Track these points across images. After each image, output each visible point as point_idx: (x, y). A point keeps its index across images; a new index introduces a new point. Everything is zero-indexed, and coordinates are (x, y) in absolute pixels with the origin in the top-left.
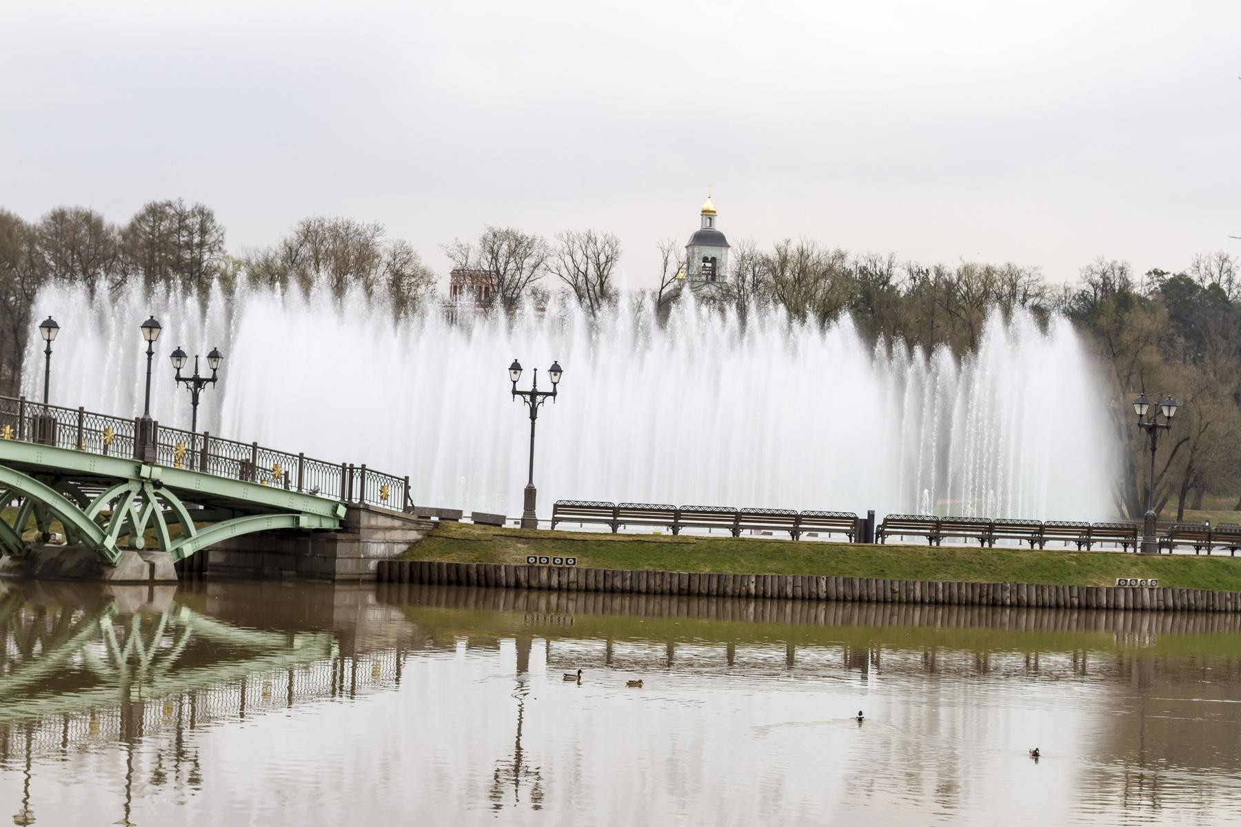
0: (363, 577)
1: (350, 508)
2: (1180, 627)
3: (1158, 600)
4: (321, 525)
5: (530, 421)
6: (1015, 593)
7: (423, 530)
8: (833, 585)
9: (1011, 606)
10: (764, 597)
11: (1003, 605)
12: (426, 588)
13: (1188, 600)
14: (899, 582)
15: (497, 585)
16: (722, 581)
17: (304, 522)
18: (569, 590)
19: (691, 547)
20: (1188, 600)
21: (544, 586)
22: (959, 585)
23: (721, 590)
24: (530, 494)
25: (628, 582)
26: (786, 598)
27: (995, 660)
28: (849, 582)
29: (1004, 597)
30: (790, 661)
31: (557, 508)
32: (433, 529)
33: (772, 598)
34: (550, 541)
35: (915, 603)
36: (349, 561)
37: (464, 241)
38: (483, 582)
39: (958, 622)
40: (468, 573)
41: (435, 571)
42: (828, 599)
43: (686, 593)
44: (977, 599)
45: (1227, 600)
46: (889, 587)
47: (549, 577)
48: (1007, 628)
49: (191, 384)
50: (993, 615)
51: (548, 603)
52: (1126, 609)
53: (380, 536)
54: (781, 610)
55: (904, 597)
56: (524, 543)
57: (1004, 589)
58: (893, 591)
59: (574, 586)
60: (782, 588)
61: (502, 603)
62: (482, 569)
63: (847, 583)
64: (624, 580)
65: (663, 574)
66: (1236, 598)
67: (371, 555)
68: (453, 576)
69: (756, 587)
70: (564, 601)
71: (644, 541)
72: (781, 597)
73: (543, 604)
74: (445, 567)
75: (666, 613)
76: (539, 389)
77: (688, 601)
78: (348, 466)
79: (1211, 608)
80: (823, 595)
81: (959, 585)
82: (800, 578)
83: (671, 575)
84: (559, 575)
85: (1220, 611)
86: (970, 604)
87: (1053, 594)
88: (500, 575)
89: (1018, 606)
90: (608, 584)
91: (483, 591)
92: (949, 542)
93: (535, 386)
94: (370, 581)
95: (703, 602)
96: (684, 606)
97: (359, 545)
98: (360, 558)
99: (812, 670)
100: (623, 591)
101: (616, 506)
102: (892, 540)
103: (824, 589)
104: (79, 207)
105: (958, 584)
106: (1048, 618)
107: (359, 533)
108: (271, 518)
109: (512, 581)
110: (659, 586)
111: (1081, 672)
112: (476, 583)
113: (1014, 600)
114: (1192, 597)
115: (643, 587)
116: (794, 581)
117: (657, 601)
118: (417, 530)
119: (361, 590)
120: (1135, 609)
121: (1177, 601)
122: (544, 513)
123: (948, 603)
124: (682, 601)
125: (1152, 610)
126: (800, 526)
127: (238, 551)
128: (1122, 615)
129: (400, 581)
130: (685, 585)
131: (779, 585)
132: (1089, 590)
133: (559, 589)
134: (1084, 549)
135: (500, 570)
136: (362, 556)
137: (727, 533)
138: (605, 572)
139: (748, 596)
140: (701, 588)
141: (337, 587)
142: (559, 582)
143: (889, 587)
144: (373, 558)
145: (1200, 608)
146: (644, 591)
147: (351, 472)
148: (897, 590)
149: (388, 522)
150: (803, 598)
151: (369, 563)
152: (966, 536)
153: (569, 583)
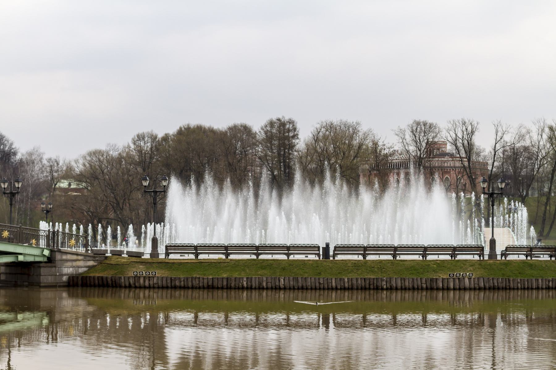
0: (59, 284)
2: (489, 299)
3: (474, 284)
4: (35, 260)
6: (389, 282)
7: (97, 260)
8: (287, 281)
9: (387, 289)
11: (382, 289)
12: (89, 288)
13: (493, 283)
14: (323, 278)
15: (121, 287)
17: (21, 258)
18: (154, 288)
19: (225, 264)
20: (493, 283)
21: (142, 286)
22: (357, 279)
23: (229, 285)
25: (182, 283)
26: (263, 288)
29: (382, 285)
30: (424, 320)
31: (335, 247)
32: (104, 260)
33: (255, 288)
34: (157, 264)
35: (332, 289)
36: (50, 276)
38: (114, 285)
39: (357, 298)
41: (92, 280)
42: (285, 289)
43: (211, 287)
44: (367, 286)
46: (317, 281)
47: (144, 281)
48: (385, 300)
49: (9, 195)
50: (377, 294)
51: (144, 294)
52: (454, 289)
53: (69, 264)
54: (260, 295)
55: (326, 286)
56: (143, 265)
58: (320, 284)
60: (261, 283)
61: (123, 295)
63: (295, 280)
64: (180, 282)
65: (199, 278)
69: (247, 283)
70: (151, 293)
71: (203, 262)
72: (261, 288)
73: (142, 295)
74: (96, 278)
75: (201, 297)
80: (282, 286)
81: (357, 279)
82: (270, 278)
83: (203, 279)
84: (149, 280)
85: (514, 289)
86: (363, 289)
87: (410, 282)
89: (390, 289)
90: (173, 284)
91: (114, 290)
94: (64, 286)
95: (220, 291)
96: (210, 294)
97: (55, 269)
98: (56, 275)
99: (434, 324)
100: (180, 288)
101: (396, 246)
102: (339, 257)
103: (283, 283)
104: (242, 123)
105: (356, 278)
106: (408, 295)
107: (55, 263)
108: (2, 257)
109: (127, 284)
110: (198, 284)
112: (111, 285)
113: (388, 286)
114: (495, 281)
116: (267, 279)
117: (197, 292)
118: (94, 261)
120: (460, 289)
121: (486, 284)
122: (161, 250)
125: (470, 289)
126: (427, 252)
127: (10, 274)
128: (452, 292)
130: (210, 283)
131: (259, 282)
132: (432, 280)
133: (149, 287)
136: (58, 274)
137: (390, 257)
139: (243, 288)
141: (42, 289)
142: (149, 284)
143: (317, 281)
144: (65, 275)
145: (195, 287)
148: (322, 282)
149: (75, 257)
150: (272, 288)
153: (154, 284)
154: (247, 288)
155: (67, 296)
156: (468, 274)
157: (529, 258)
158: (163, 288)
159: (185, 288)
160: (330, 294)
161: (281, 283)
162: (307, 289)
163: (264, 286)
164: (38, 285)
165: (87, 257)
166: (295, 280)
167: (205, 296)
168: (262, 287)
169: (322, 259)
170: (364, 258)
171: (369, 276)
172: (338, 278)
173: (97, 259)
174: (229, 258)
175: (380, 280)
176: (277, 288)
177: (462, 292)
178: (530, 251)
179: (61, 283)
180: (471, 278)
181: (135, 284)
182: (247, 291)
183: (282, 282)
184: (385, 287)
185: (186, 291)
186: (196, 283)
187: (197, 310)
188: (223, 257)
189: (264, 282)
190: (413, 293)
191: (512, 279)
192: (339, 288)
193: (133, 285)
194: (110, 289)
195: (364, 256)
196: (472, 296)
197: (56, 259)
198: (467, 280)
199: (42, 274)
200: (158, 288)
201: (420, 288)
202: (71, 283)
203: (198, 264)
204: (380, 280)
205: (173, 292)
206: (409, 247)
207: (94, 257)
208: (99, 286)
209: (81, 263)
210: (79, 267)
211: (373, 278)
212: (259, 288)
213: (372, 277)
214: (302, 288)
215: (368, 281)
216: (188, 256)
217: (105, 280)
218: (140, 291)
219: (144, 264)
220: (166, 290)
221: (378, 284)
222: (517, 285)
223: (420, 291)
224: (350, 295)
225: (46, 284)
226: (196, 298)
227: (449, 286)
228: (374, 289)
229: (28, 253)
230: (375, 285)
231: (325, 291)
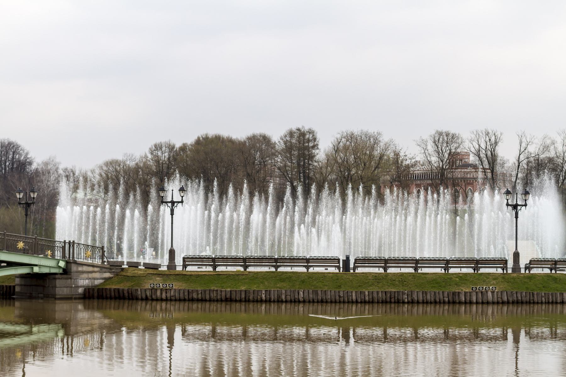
0: (74, 296)
1: (67, 263)
2: (512, 312)
3: (497, 298)
4: (50, 271)
5: (171, 216)
7: (114, 272)
8: (306, 294)
10: (270, 301)
11: (404, 303)
12: (105, 301)
13: (517, 297)
15: (137, 299)
16: (247, 294)
17: (36, 270)
18: (171, 300)
20: (517, 297)
21: (159, 299)
22: (378, 292)
23: (247, 298)
24: (172, 253)
26: (282, 301)
27: (251, 330)
28: (316, 292)
32: (120, 272)
33: (274, 301)
37: (424, 138)
38: (131, 297)
40: (123, 293)
41: (108, 293)
42: (304, 302)
43: (229, 300)
44: (388, 300)
45: (542, 297)
46: (337, 294)
47: (161, 294)
48: (406, 315)
50: (398, 307)
51: (161, 306)
52: (477, 303)
53: (85, 275)
54: (279, 308)
55: (346, 299)
56: (160, 277)
57: (403, 293)
58: (340, 296)
59: (173, 298)
62: (130, 291)
63: (314, 293)
64: (198, 294)
65: (217, 290)
66: (548, 296)
67: (79, 285)
68: (117, 295)
69: (265, 296)
70: (168, 306)
71: (221, 274)
72: (279, 301)
73: (158, 307)
75: (219, 310)
76: (175, 200)
77: (231, 305)
78: (72, 242)
79: (532, 301)
80: (301, 299)
81: (378, 292)
83: (221, 291)
84: (166, 293)
85: (538, 303)
86: (384, 302)
87: (432, 296)
88: (138, 294)
90: (190, 297)
91: (131, 302)
92: (536, 271)
93: (172, 198)
94: (80, 298)
96: (228, 307)
100: (198, 300)
102: (360, 270)
106: (429, 308)
107: (71, 275)
108: (17, 268)
109: (144, 296)
110: (215, 297)
111: (554, 336)
112: (127, 298)
113: (410, 299)
114: (519, 295)
115: (208, 297)
117: (215, 305)
118: (110, 272)
119: (73, 303)
120: (483, 303)
121: (509, 298)
122: (179, 261)
123: (371, 302)
124: (228, 304)
125: (493, 303)
126: (449, 265)
127: (25, 285)
129: (94, 298)
130: (228, 296)
131: (278, 295)
132: (454, 294)
133: (166, 300)
134: (553, 272)
135: (138, 291)
136: (73, 286)
137: (411, 270)
138: (188, 291)
139: (262, 301)
140: (237, 297)
141: (57, 302)
142: (166, 296)
144: (81, 287)
146: (208, 300)
147: (73, 246)
148: (342, 295)
149: (91, 269)
151: (78, 289)
152: (543, 267)
153: (171, 297)
155: (83, 308)
156: (491, 287)
157: (553, 272)
158: (180, 300)
159: (203, 300)
160: (350, 308)
162: (327, 302)
163: (283, 299)
165: (103, 269)
166: (314, 293)
169: (343, 271)
170: (385, 271)
172: (358, 291)
173: (113, 270)
174: (247, 270)
175: (401, 293)
176: (296, 302)
177: (485, 306)
179: (77, 295)
180: (494, 292)
183: (301, 295)
184: (406, 300)
185: (204, 304)
186: (213, 295)
188: (241, 269)
189: (283, 295)
192: (360, 301)
193: (150, 298)
195: (385, 269)
197: (72, 271)
198: (490, 294)
200: (176, 300)
201: (442, 301)
204: (401, 293)
205: (190, 305)
207: (111, 269)
208: (115, 298)
209: (97, 275)
210: (95, 279)
212: (278, 301)
214: (322, 301)
215: (389, 294)
216: (227, 268)
217: (121, 292)
219: (161, 276)
220: (200, 304)
221: (399, 298)
224: (371, 309)
225: (62, 296)
227: (471, 300)
228: (395, 302)
230: (396, 298)
231: (478, 305)
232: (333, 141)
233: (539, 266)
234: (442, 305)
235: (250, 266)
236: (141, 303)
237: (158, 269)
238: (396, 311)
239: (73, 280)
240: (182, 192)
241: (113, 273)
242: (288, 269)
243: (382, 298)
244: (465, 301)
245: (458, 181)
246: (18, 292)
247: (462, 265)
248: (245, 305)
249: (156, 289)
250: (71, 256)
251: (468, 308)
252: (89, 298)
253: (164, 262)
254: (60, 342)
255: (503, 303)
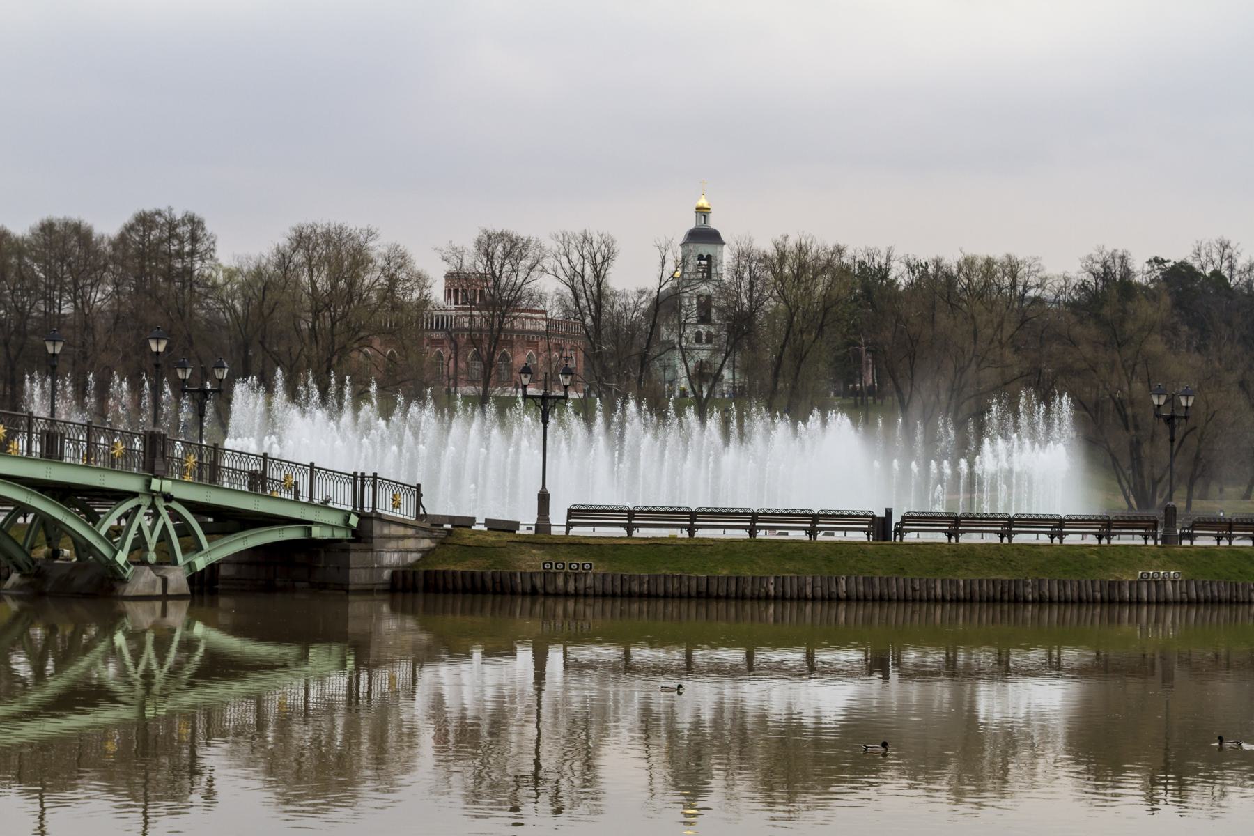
2: (1204, 619)
3: (1181, 593)
4: (333, 535)
7: (436, 538)
8: (853, 585)
9: (1034, 601)
10: (784, 598)
11: (1026, 601)
12: (441, 597)
13: (1212, 591)
15: (513, 592)
17: (317, 532)
18: (586, 595)
20: (1212, 591)
21: (561, 592)
22: (980, 582)
23: (740, 591)
24: (544, 499)
25: (646, 585)
26: (806, 599)
28: (869, 581)
32: (446, 536)
33: (791, 599)
35: (936, 600)
38: (499, 589)
39: (980, 619)
41: (450, 579)
42: (848, 599)
43: (704, 595)
47: (566, 583)
52: (1149, 603)
53: (393, 545)
54: (801, 611)
55: (925, 595)
56: (539, 549)
58: (914, 590)
59: (591, 591)
60: (802, 589)
64: (641, 584)
65: (680, 577)
70: (581, 607)
71: (660, 544)
72: (801, 598)
73: (560, 610)
78: (359, 474)
80: (843, 595)
81: (980, 582)
83: (689, 578)
84: (576, 581)
85: (1244, 602)
86: (992, 601)
87: (1075, 589)
89: (1040, 601)
90: (626, 588)
91: (499, 598)
94: (385, 591)
95: (722, 605)
96: (703, 610)
97: (372, 555)
98: (373, 568)
100: (641, 596)
102: (910, 537)
104: (67, 217)
106: (1071, 613)
107: (372, 542)
108: (282, 529)
109: (528, 587)
113: (1036, 595)
114: (1215, 588)
115: (661, 590)
118: (430, 538)
120: (1158, 602)
122: (558, 518)
123: (970, 600)
125: (1175, 602)
126: (818, 526)
130: (703, 587)
131: (798, 586)
132: (1111, 584)
133: (576, 595)
136: (376, 566)
137: (744, 534)
138: (622, 576)
141: (351, 598)
142: (576, 587)
144: (387, 568)
147: (363, 481)
148: (918, 588)
149: (401, 531)
151: (383, 572)
152: (982, 532)
153: (585, 589)
154: (775, 598)
158: (604, 595)
159: (650, 596)
161: (840, 588)
162: (890, 600)
164: (343, 588)
165: (420, 532)
167: (693, 612)
168: (803, 596)
169: (873, 539)
170: (691, 534)
171: (999, 577)
173: (436, 534)
175: (1021, 584)
176: (833, 599)
177: (1162, 608)
178: (1106, 526)
179: (380, 584)
181: (544, 588)
182: (848, 605)
183: (842, 586)
184: (1030, 597)
185: (653, 603)
186: (673, 586)
187: (625, 639)
189: (808, 587)
190: (1079, 610)
191: (1240, 584)
192: (948, 598)
193: (541, 591)
194: (490, 598)
195: (691, 530)
196: (852, 617)
198: (1169, 585)
199: (352, 566)
200: (595, 596)
201: (1091, 599)
202: (400, 584)
203: (651, 547)
204: (1021, 584)
206: (1034, 519)
207: (431, 531)
208: (465, 591)
209: (410, 544)
211: (531, 573)
212: (799, 598)
213: (1006, 578)
214: (881, 599)
218: (555, 604)
220: (646, 603)
222: (1249, 594)
223: (991, 604)
224: (968, 613)
225: (358, 587)
226: (672, 617)
228: (1009, 601)
229: (323, 522)
230: (1013, 593)
232: (281, 246)
233: (975, 528)
234: (870, 604)
235: (1017, 532)
236: (920, 608)
237: (470, 527)
238: (1012, 616)
239: (375, 553)
240: (526, 377)
241: (434, 540)
242: (717, 534)
243: (988, 593)
244: (1130, 599)
245: (512, 336)
246: (225, 578)
247: (984, 529)
248: (752, 607)
249: (555, 574)
250: (358, 505)
251: (917, 607)
252: (405, 590)
253: (527, 517)
254: (871, 678)
255: (1190, 602)
